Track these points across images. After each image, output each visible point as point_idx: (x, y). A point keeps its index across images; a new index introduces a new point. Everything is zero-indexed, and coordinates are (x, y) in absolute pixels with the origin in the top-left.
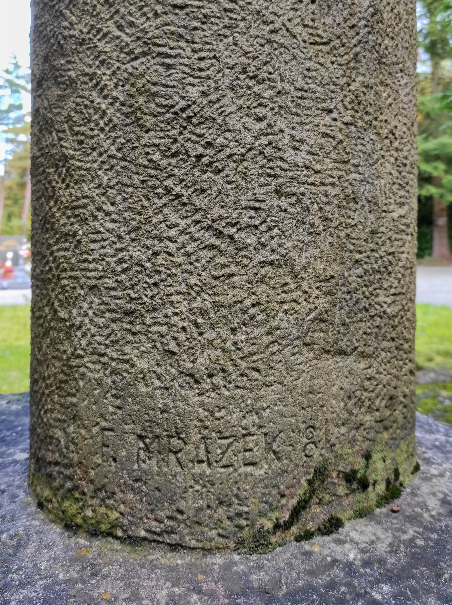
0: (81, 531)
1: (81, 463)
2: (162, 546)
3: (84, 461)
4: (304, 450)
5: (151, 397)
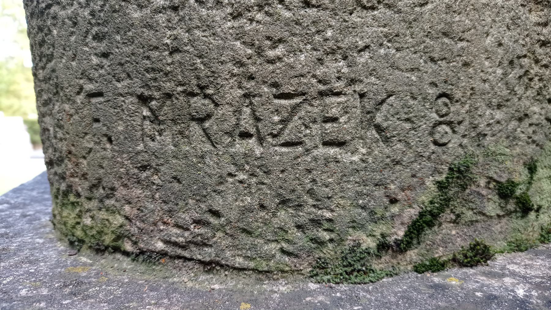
0: (85, 247)
1: (70, 153)
2: (190, 264)
3: (73, 148)
4: (431, 134)
5: (149, 26)
